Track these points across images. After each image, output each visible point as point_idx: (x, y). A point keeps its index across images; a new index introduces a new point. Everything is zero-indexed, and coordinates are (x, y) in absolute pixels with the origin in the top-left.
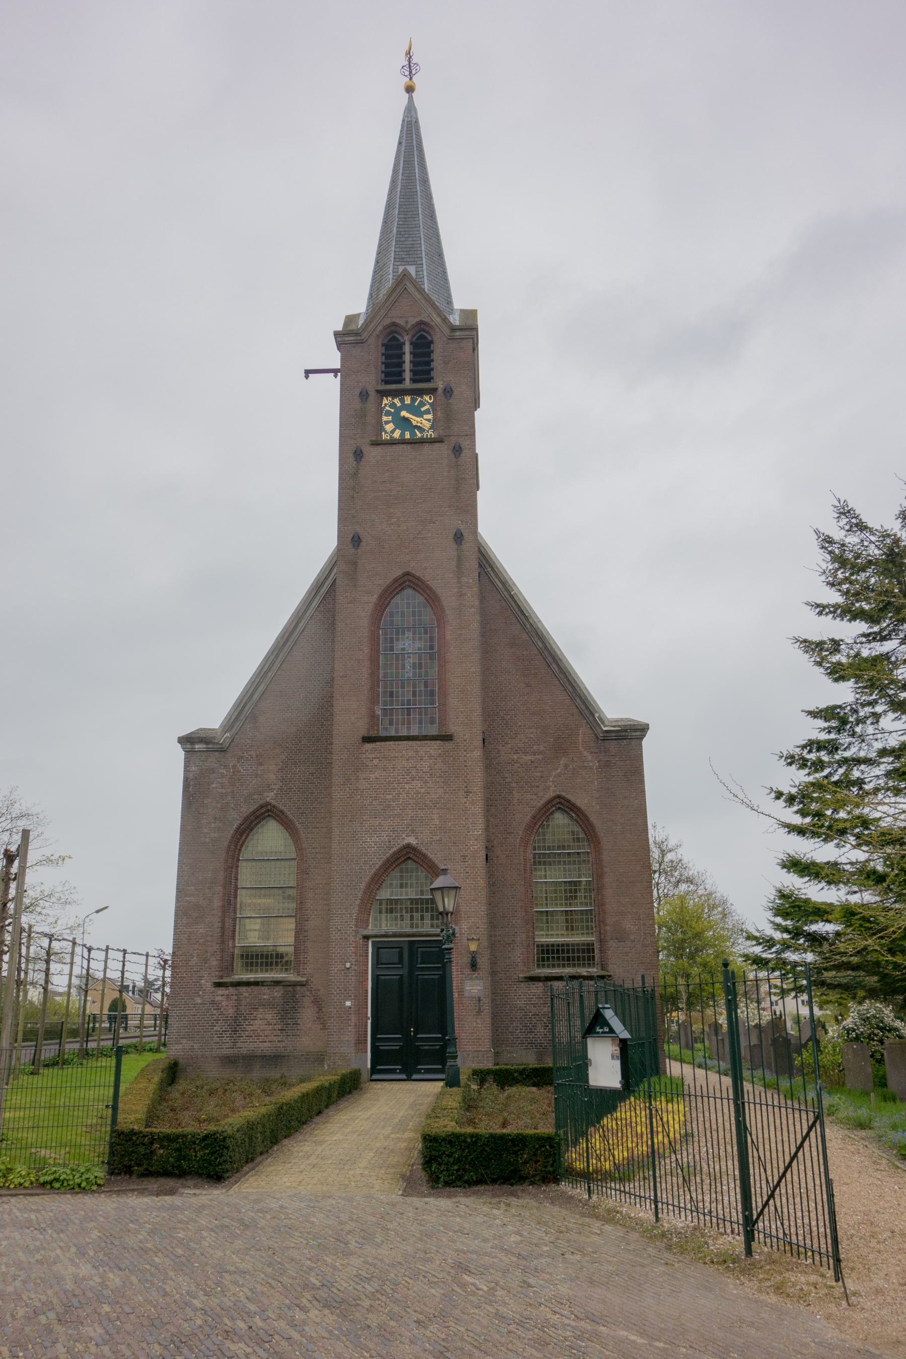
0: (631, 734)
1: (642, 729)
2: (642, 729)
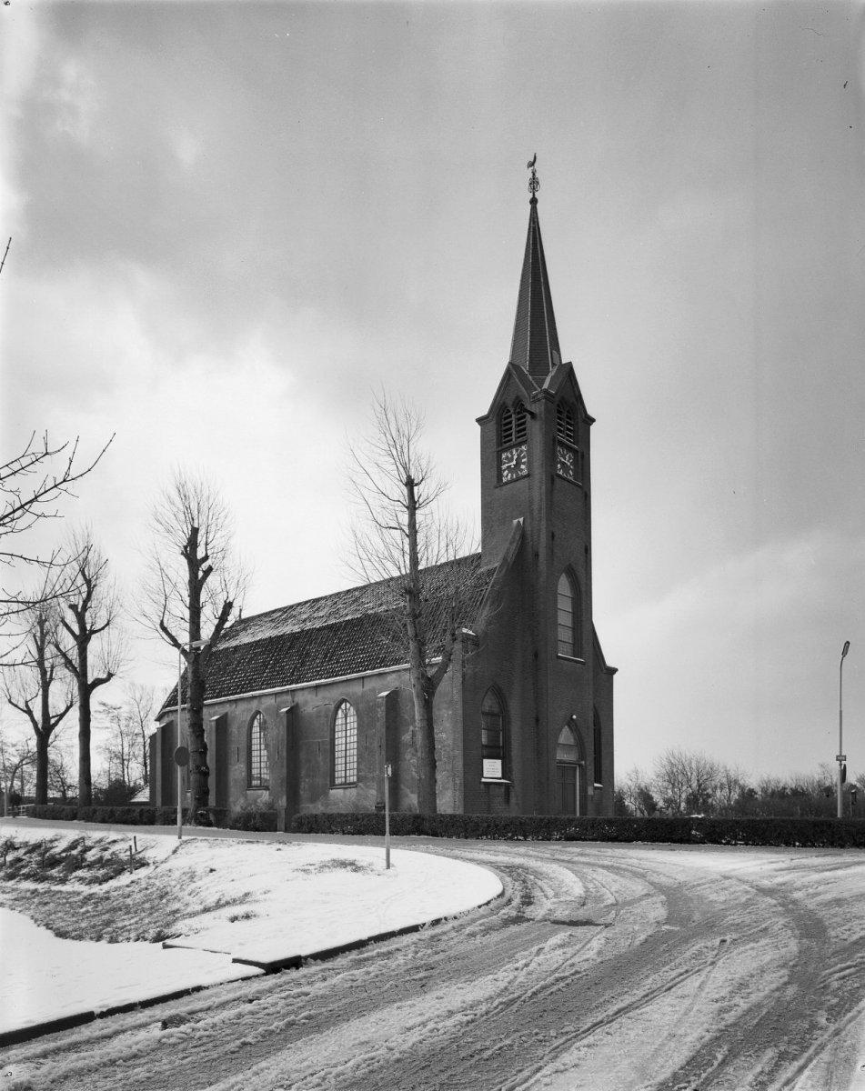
0: (614, 671)
1: (593, 420)
2: (593, 420)
